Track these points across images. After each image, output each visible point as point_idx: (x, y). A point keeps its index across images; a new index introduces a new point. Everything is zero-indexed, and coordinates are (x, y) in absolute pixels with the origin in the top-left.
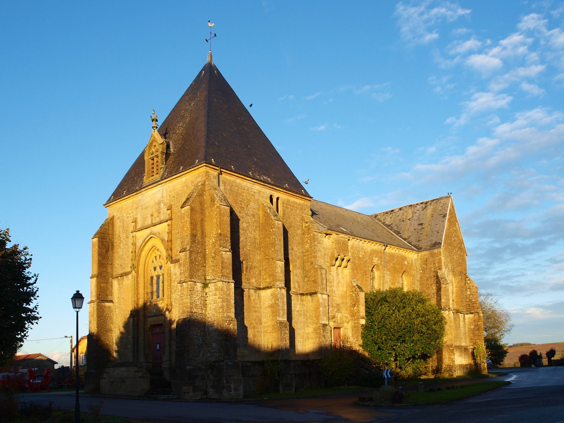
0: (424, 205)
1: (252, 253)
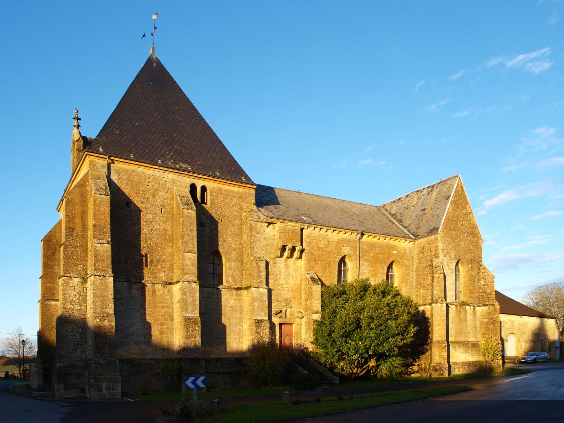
0: (430, 189)
1: (161, 246)
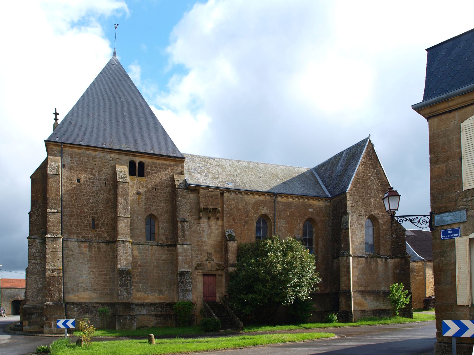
1: (105, 212)
